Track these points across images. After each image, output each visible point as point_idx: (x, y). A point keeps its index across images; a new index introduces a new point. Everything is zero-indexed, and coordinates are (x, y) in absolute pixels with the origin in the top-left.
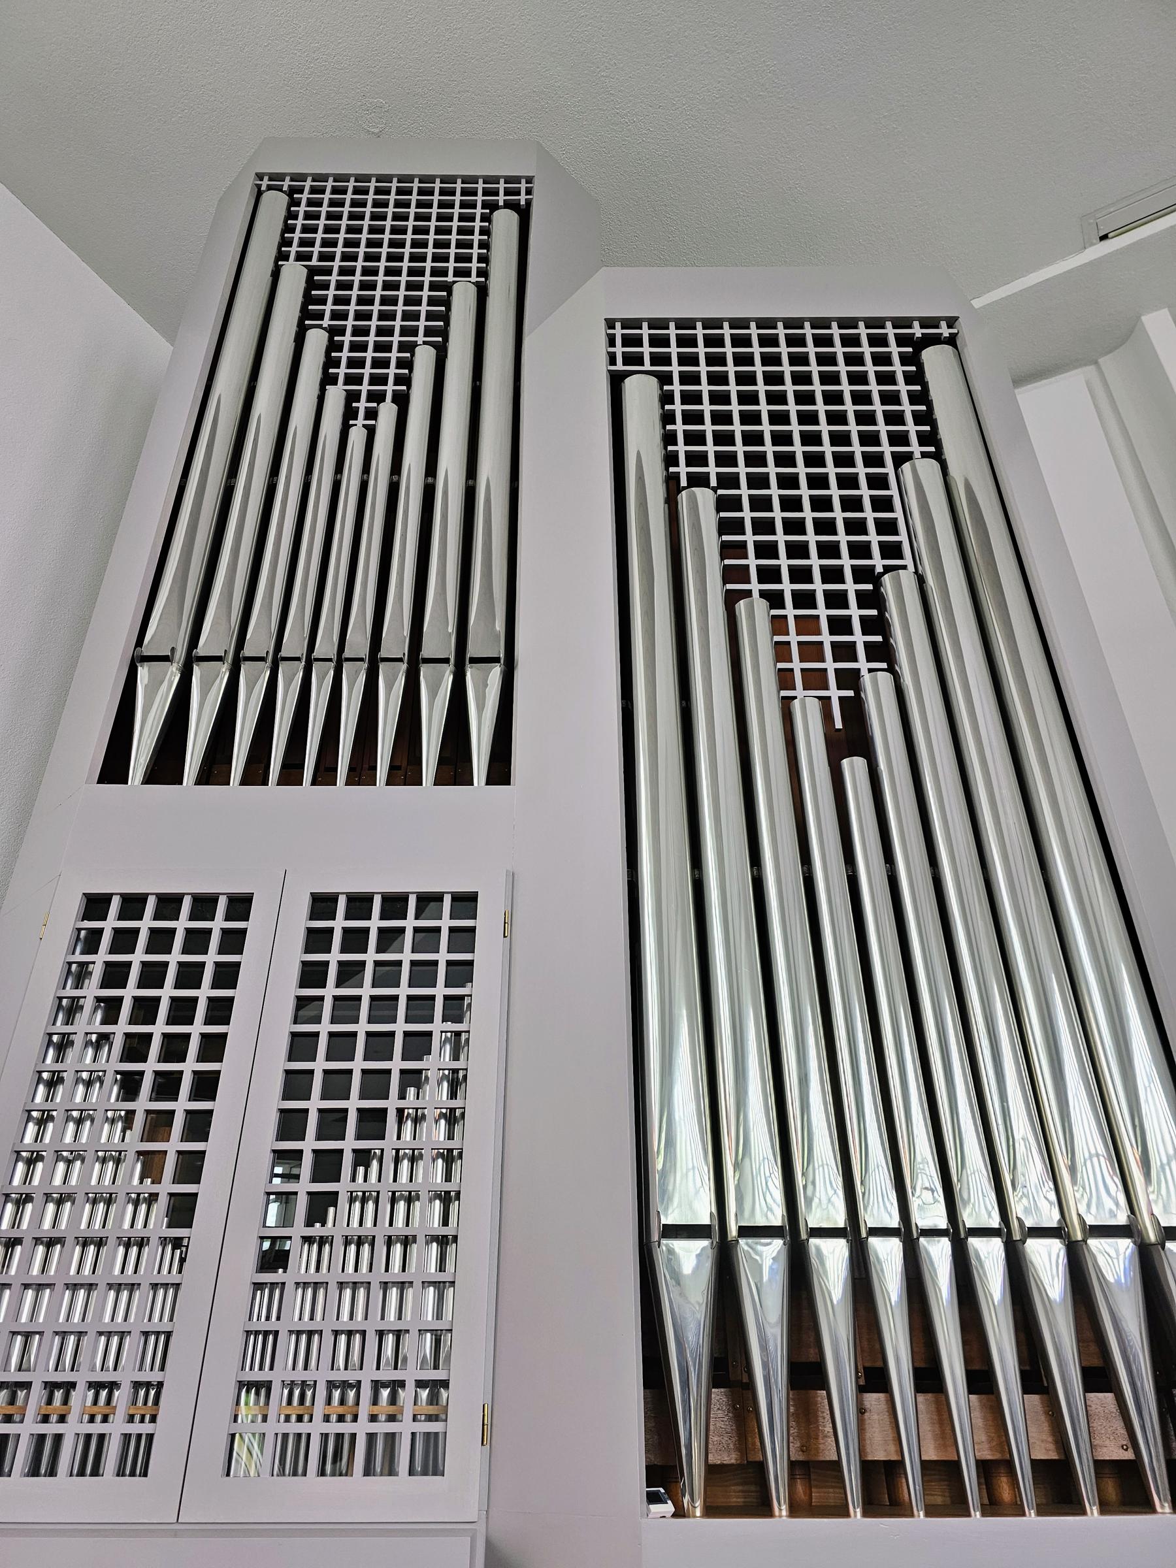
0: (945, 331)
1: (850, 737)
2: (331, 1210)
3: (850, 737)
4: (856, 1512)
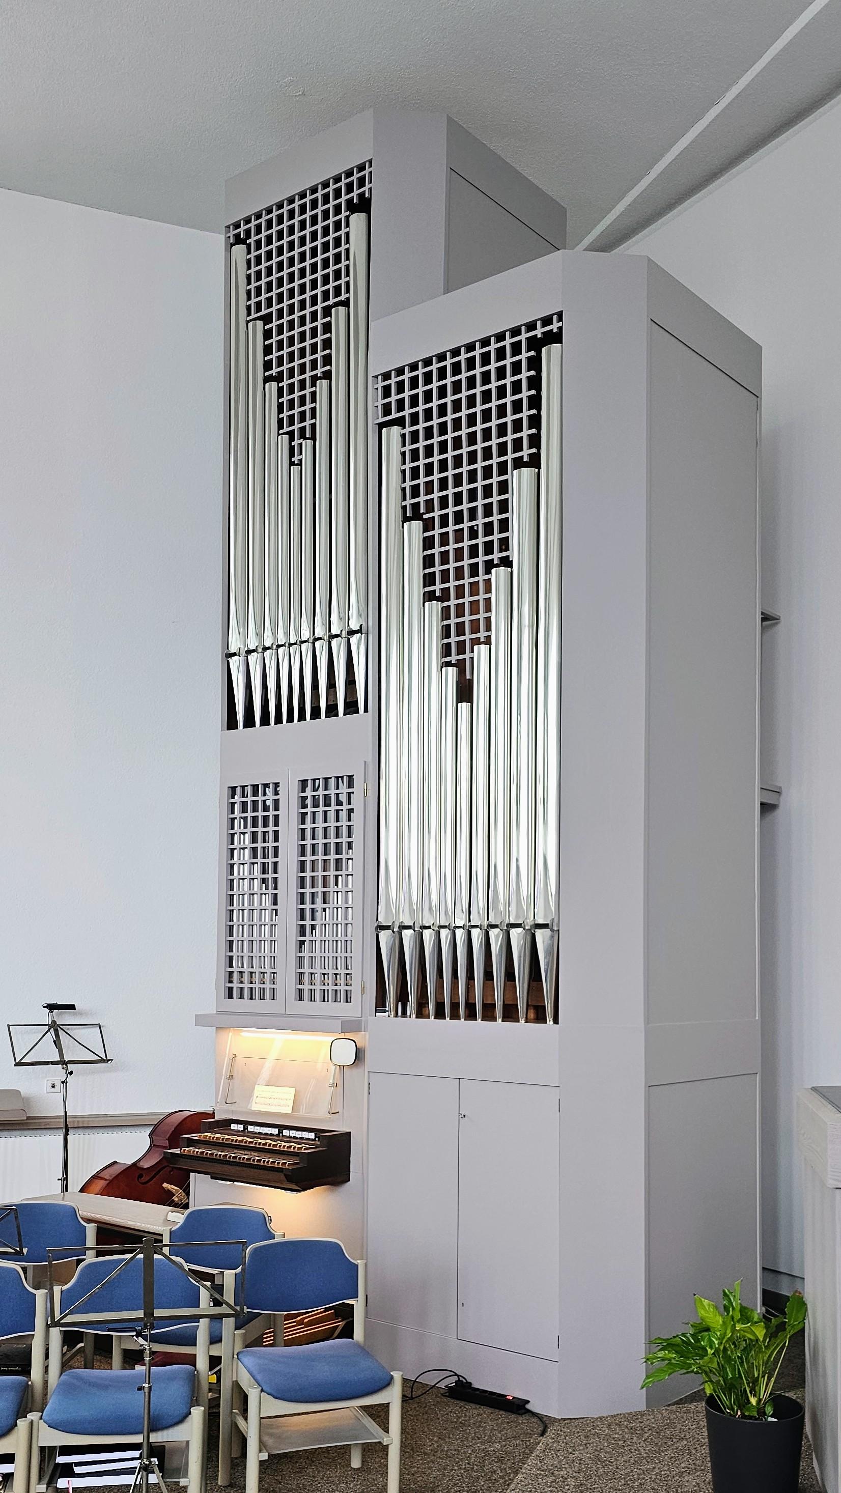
0: (554, 327)
1: (465, 692)
2: (521, 481)
3: (465, 692)
4: (522, 1021)
